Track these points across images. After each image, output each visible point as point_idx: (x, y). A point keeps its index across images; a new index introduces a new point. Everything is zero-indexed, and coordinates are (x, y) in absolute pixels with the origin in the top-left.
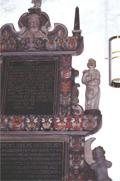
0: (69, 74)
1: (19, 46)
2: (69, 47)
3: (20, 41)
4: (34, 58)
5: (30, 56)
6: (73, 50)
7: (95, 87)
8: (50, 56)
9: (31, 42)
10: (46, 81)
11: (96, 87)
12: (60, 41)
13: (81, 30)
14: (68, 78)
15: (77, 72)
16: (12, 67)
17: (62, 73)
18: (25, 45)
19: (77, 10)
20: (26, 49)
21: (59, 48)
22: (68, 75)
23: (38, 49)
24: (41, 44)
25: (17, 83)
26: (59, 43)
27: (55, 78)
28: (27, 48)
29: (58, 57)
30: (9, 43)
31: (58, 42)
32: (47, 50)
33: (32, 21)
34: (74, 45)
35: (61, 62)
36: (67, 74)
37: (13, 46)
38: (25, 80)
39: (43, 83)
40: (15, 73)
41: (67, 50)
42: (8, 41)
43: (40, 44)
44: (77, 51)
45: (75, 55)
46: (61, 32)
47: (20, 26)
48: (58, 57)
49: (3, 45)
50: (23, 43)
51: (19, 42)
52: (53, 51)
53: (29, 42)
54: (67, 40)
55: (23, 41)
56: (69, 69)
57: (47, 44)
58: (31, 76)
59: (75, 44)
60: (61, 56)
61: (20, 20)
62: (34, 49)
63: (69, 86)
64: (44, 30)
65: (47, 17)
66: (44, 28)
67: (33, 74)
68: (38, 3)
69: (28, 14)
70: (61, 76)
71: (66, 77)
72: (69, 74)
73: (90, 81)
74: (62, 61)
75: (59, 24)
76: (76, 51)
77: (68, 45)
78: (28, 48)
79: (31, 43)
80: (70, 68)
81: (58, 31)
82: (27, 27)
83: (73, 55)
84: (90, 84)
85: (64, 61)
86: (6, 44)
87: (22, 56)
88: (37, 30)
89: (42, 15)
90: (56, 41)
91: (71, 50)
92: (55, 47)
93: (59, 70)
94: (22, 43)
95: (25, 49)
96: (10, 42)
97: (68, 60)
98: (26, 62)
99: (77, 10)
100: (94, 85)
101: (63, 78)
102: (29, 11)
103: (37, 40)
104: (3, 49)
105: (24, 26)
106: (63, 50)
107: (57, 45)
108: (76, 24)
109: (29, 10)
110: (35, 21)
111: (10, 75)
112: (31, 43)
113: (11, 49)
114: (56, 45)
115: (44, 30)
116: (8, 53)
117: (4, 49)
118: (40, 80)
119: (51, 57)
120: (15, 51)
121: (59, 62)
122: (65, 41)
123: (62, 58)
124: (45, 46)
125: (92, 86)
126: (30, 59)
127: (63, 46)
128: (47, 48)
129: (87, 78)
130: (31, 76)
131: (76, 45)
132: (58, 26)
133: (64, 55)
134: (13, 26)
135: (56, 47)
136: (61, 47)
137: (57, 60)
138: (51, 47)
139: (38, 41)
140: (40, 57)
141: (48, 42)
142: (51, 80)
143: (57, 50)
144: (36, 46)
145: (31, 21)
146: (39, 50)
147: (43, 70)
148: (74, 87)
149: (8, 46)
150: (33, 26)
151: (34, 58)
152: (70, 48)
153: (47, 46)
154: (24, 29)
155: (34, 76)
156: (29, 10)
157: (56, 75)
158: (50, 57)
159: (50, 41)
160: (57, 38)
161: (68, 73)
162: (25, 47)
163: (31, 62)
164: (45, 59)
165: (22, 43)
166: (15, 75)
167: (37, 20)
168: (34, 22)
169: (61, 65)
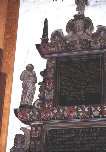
3: (69, 44)
5: (78, 56)
9: (78, 43)
12: (103, 41)
16: (63, 66)
18: (73, 46)
20: (75, 50)
21: (102, 47)
24: (87, 44)
28: (74, 49)
29: (102, 55)
31: (101, 41)
32: (92, 49)
33: (78, 25)
37: (63, 48)
40: (66, 70)
42: (58, 44)
43: (86, 44)
47: (68, 31)
48: (102, 55)
53: (76, 44)
57: (91, 44)
61: (67, 26)
62: (81, 49)
64: (88, 32)
65: (91, 21)
66: (88, 31)
68: (82, 9)
75: (101, 26)
78: (76, 49)
81: (101, 32)
82: (74, 31)
87: (72, 56)
93: (104, 65)
95: (73, 50)
98: (74, 61)
109: (74, 16)
114: (99, 44)
120: (65, 52)
124: (90, 46)
126: (78, 58)
132: (100, 27)
138: (95, 46)
139: (84, 42)
143: (100, 49)
144: (82, 46)
145: (77, 25)
146: (85, 49)
147: (90, 66)
150: (79, 30)
151: (81, 57)
153: (92, 46)
154: (71, 33)
156: (74, 16)
159: (94, 41)
162: (73, 48)
163: (79, 60)
167: (81, 25)
168: (79, 26)
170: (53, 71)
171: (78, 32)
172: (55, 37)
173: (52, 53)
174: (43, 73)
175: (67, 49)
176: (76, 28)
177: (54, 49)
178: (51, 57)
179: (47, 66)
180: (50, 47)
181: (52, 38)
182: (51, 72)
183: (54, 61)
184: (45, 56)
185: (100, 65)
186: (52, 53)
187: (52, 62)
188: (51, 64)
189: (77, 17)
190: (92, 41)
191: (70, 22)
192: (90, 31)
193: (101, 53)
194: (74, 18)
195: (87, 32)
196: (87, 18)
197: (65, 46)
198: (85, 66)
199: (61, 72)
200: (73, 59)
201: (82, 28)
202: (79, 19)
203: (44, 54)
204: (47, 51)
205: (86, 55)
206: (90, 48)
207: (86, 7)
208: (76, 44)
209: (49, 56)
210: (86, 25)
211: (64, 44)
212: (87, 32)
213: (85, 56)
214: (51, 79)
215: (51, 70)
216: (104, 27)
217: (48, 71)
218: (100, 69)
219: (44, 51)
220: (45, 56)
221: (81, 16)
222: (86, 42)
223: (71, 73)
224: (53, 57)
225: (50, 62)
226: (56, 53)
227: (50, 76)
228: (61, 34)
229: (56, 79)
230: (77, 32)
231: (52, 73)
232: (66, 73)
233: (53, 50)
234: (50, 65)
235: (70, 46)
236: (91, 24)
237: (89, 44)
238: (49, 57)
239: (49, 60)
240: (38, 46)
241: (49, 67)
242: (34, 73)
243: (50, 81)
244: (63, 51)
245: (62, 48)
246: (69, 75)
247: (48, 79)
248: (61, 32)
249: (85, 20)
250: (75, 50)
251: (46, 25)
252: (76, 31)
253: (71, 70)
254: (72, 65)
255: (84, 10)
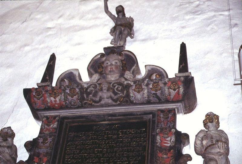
0: (171, 139)
1: (85, 96)
2: (170, 95)
3: (87, 89)
4: (110, 118)
5: (104, 115)
6: (178, 102)
7: (220, 155)
8: (139, 114)
9: (104, 88)
10: (131, 154)
11: (222, 156)
12: (153, 85)
13: (190, 73)
14: (169, 145)
15: (186, 136)
16: (72, 134)
17: (158, 138)
18: (95, 95)
19: (183, 47)
20: (97, 102)
21: (151, 98)
22: (170, 141)
23: (116, 102)
24: (122, 91)
25: (80, 159)
26: (151, 88)
27: (146, 148)
28: (97, 99)
29: (151, 115)
30: (69, 92)
31: (151, 86)
32: (132, 103)
33: (109, 64)
34: (178, 91)
35: (156, 121)
36: (167, 139)
37: (75, 97)
38: (94, 153)
39: (124, 157)
40: (77, 142)
41: (167, 101)
42: (66, 89)
43: (119, 91)
44: (185, 104)
45: (181, 112)
46: (156, 75)
47: (90, 75)
48: (151, 115)
49: (59, 97)
50: (92, 91)
51: (85, 90)
52: (142, 104)
53: (101, 90)
54: (165, 84)
55: (91, 88)
56: (170, 131)
57: (131, 91)
58: (105, 146)
59: (179, 88)
60: (156, 113)
61: (91, 65)
62: (110, 101)
63: (172, 159)
64: (129, 77)
65: (135, 59)
66: (128, 75)
67: (108, 143)
68: (120, 41)
69: (102, 55)
70: (157, 143)
71: (166, 145)
72: (171, 139)
73: (210, 146)
74: (158, 119)
75: (154, 67)
76: (183, 102)
77: (167, 90)
78: (100, 100)
79: (105, 90)
80: (173, 130)
81: (152, 74)
82: (101, 74)
83: (178, 112)
84: (209, 151)
85: (162, 119)
86: (63, 94)
87: (92, 116)
88: (118, 78)
89: (126, 55)
90: (147, 85)
91: (173, 102)
92: (146, 95)
93: (153, 134)
94: (89, 91)
95: (95, 102)
96: (70, 90)
97: (168, 118)
98: (96, 125)
99: (183, 47)
100: (217, 153)
101: (160, 146)
102: (104, 51)
103: (115, 85)
104: (58, 104)
105: (96, 72)
106: (160, 102)
107: (148, 92)
108: (181, 66)
109: (105, 49)
110: (113, 63)
111: (69, 145)
112: (105, 90)
113: (71, 104)
114: (146, 91)
115: (129, 77)
116: (67, 111)
117: (60, 103)
118: (119, 152)
119: (140, 115)
120: (78, 107)
121: (154, 122)
122: (162, 85)
123: (158, 115)
124: (128, 95)
125: (213, 154)
126: (104, 121)
127: (159, 93)
128: (132, 99)
129: (205, 142)
130: (105, 146)
131: (182, 90)
132: (152, 69)
133: (162, 111)
134: (79, 74)
135: (148, 96)
136: (156, 94)
137: (150, 119)
138: (139, 96)
139: (116, 87)
140: (121, 116)
141: (134, 87)
142: (139, 151)
143: (149, 102)
144: (113, 95)
145: (107, 63)
146: (119, 102)
147: (126, 135)
148: (181, 161)
149: (67, 97)
150: (110, 71)
151: (110, 118)
152: (172, 97)
153: (132, 95)
154: (96, 77)
155: (109, 146)
156: (105, 49)
157: (149, 143)
158: (137, 115)
159: (136, 86)
160: (148, 80)
161: (169, 138)
162: (94, 98)
163: (106, 124)
164: (130, 119)
165: (89, 91)
166: (77, 145)
167: (116, 63)
168: (112, 64)
169: (157, 126)
170: (50, 142)
171: (109, 76)
172: (65, 80)
173: (52, 108)
174: (30, 146)
175: (82, 99)
176: (106, 67)
177: (57, 99)
178: (52, 116)
179: (40, 133)
180: (50, 94)
181: (58, 82)
182: (48, 142)
183: (56, 123)
184: (39, 115)
185: (146, 135)
186: (52, 108)
187: (52, 126)
188: (48, 128)
189: (108, 51)
190: (132, 86)
191: (96, 58)
192: (132, 75)
193: (151, 113)
194: (104, 53)
195: (126, 76)
196: (127, 53)
197: (79, 92)
198: (115, 136)
199: (66, 145)
200: (93, 121)
201: (117, 67)
202: (113, 54)
203: (38, 110)
204: (44, 101)
205: (119, 115)
206: (127, 101)
207: (129, 42)
208: (101, 90)
209: (48, 114)
210: (125, 64)
211: (77, 90)
212: (126, 76)
213: (119, 117)
214: (45, 156)
215: (47, 140)
216: (159, 68)
217: (41, 140)
218: (145, 141)
219: (38, 103)
220: (40, 114)
221: (116, 49)
222: (120, 87)
223: (87, 147)
224: (55, 117)
225: (47, 125)
226: (61, 107)
227: (43, 150)
228: (78, 79)
229: (55, 157)
230: (108, 76)
231: (48, 144)
232: (76, 147)
233: (55, 101)
234: (47, 129)
235: (88, 94)
236: (135, 63)
237: (125, 92)
238: (47, 118)
239: (46, 122)
240: (27, 93)
241: (44, 133)
242: (10, 142)
243: (40, 158)
244: (74, 103)
245: (72, 97)
246: (83, 151)
247: (38, 155)
248: (77, 75)
249: (124, 56)
250: (96, 103)
251: (51, 63)
252: (106, 74)
253: (89, 142)
254: (91, 134)
255: (125, 41)
